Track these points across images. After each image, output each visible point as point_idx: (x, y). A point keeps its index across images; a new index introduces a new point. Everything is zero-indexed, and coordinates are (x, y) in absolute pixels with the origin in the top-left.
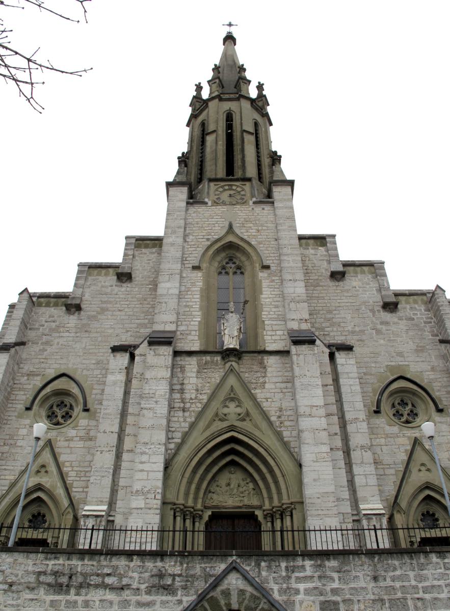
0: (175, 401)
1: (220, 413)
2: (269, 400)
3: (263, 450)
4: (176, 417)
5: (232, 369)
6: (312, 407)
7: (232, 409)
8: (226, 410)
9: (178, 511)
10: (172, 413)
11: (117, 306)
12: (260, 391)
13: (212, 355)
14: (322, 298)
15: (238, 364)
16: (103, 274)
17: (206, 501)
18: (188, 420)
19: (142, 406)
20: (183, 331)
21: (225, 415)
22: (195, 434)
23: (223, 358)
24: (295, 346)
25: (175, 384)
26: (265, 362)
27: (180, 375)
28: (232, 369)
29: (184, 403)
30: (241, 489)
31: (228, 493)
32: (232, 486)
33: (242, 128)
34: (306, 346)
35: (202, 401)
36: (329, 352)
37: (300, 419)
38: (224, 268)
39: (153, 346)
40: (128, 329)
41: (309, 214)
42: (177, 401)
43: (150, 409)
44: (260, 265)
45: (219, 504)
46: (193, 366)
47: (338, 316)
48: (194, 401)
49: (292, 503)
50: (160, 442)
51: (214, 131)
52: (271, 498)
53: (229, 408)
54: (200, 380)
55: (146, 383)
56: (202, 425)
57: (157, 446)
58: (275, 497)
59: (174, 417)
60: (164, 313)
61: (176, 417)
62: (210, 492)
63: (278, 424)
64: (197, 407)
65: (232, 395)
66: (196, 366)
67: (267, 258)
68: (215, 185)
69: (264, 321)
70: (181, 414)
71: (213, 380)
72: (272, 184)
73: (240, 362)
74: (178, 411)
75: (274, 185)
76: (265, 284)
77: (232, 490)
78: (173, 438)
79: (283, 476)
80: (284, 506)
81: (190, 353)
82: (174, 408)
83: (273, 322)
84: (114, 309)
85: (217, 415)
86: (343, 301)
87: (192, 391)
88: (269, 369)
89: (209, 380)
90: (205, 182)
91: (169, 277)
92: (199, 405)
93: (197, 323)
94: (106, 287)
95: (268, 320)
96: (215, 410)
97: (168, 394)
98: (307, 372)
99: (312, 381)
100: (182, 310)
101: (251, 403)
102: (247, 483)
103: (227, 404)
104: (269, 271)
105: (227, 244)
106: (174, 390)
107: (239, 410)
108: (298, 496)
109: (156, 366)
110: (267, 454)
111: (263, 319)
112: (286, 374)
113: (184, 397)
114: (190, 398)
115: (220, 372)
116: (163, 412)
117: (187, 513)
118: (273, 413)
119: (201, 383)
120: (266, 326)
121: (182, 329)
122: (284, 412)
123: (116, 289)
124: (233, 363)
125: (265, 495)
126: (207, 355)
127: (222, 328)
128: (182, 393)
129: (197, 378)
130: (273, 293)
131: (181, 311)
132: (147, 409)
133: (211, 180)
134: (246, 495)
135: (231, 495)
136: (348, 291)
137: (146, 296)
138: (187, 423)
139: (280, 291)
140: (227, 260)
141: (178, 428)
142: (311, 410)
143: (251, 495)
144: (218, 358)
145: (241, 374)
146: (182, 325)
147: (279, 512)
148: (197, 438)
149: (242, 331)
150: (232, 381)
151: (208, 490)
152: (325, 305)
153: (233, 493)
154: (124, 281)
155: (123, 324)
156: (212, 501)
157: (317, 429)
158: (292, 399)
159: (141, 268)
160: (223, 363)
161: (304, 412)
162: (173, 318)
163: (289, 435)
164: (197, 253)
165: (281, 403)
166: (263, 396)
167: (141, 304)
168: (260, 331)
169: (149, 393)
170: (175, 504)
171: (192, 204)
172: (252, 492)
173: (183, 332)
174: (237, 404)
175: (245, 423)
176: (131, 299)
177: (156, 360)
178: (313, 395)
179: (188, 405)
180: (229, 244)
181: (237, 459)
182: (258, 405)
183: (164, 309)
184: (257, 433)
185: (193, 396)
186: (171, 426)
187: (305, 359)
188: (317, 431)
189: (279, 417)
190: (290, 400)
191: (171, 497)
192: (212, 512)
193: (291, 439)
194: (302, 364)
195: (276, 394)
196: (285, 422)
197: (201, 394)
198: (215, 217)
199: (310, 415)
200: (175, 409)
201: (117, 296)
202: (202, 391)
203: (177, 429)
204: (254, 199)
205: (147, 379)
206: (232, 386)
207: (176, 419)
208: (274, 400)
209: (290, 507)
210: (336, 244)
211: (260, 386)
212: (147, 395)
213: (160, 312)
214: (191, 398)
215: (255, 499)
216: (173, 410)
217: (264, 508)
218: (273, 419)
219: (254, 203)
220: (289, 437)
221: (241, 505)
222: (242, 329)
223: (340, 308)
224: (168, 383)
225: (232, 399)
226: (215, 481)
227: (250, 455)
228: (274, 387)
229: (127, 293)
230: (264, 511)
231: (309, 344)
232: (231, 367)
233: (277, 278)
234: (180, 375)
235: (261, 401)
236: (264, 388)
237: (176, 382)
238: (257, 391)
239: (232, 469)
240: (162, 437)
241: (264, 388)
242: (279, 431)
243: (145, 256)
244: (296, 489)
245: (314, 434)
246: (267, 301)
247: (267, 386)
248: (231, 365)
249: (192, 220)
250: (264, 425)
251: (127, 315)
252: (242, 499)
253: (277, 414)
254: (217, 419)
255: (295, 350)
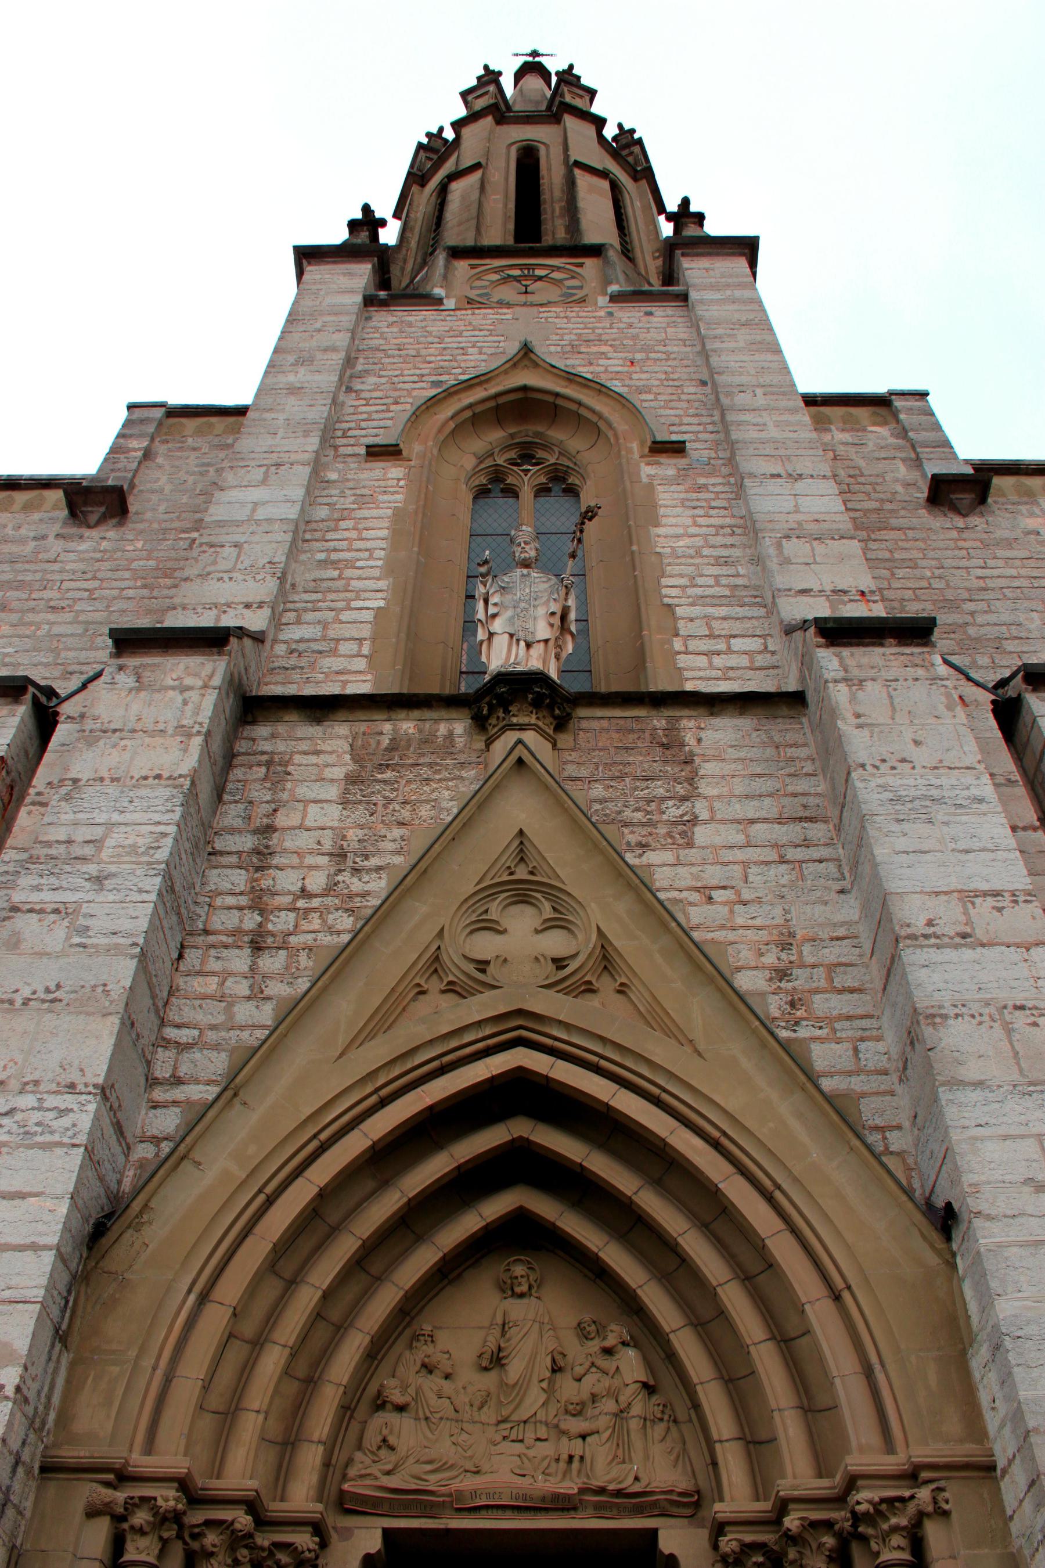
0: (219, 901)
1: (451, 955)
2: (718, 895)
3: (697, 1142)
4: (214, 974)
5: (520, 761)
6: (969, 896)
7: (522, 938)
8: (485, 946)
9: (141, 1531)
10: (192, 957)
11: (47, 594)
12: (668, 856)
13: (428, 714)
14: (911, 564)
15: (554, 746)
16: (17, 506)
17: (350, 1462)
18: (277, 989)
19: (17, 897)
20: (301, 641)
21: (482, 965)
22: (303, 1053)
23: (480, 723)
24: (832, 650)
25: (232, 831)
26: (690, 739)
27: (260, 793)
28: (520, 761)
29: (262, 912)
30: (568, 1389)
31: (489, 1415)
32: (515, 1369)
33: (567, 157)
34: (888, 651)
35: (358, 902)
36: (993, 702)
37: (912, 956)
38: (497, 476)
39: (133, 654)
40: (71, 668)
41: (823, 329)
42: (230, 901)
43: (56, 911)
44: (642, 443)
45: (433, 1482)
46: (331, 759)
47: (991, 618)
48: (316, 902)
49: (912, 1475)
50: (75, 1076)
51: (477, 166)
52: (757, 1444)
53: (504, 932)
54: (360, 814)
55: (67, 798)
56: (346, 1009)
57: (51, 1101)
58: (790, 1431)
59: (200, 973)
60: (226, 576)
61: (214, 974)
62: (380, 1404)
63: (775, 1006)
64: (331, 931)
65: (521, 873)
66: (348, 757)
67: (672, 428)
68: (473, 267)
69: (669, 605)
70: (239, 960)
71: (425, 811)
72: (678, 252)
73: (564, 739)
74: (226, 947)
75: (683, 255)
76: (667, 497)
77: (518, 1389)
78: (177, 1081)
79: (837, 1298)
80: (865, 1497)
81: (321, 708)
82: (206, 932)
83: (710, 610)
84: (32, 604)
85: (435, 964)
86: (996, 572)
87: (309, 860)
88: (708, 768)
89: (405, 814)
90: (441, 258)
91: (266, 473)
92: (346, 922)
93: (369, 616)
94: (23, 541)
95: (692, 605)
96: (427, 934)
97: (169, 842)
98: (912, 745)
99: (944, 781)
100: (308, 576)
101: (623, 906)
102: (608, 1352)
103: (495, 910)
104: (682, 462)
105: (512, 397)
106: (221, 853)
107: (556, 943)
108: (953, 1425)
109: (134, 731)
110: (728, 1168)
111: (666, 600)
112: (802, 785)
113: (265, 883)
114: (296, 888)
115: (462, 778)
116: (126, 925)
117: (211, 1539)
118: (746, 955)
119: (362, 827)
120: (681, 624)
121: (297, 637)
122: (806, 949)
123: (56, 546)
124: (530, 737)
125: (721, 1421)
126: (402, 714)
127: (481, 615)
128: (258, 869)
129: (344, 803)
130: (701, 521)
131: (302, 576)
132: (41, 911)
133: (457, 253)
134: (603, 1422)
135: (510, 1427)
136: (1009, 543)
137: (169, 565)
138: (268, 1008)
139: (734, 516)
140: (512, 454)
141: (213, 1027)
142: (966, 913)
143: (634, 1424)
144: (457, 727)
145: (568, 786)
146: (298, 622)
147: (829, 1541)
148: (313, 1079)
149: (573, 628)
150: (520, 810)
151: (372, 1389)
152: (925, 584)
153: (524, 1413)
154: (93, 518)
155: (56, 651)
156: (388, 1459)
157: (1022, 1008)
158: (842, 892)
159: (168, 488)
160: (481, 745)
161: (930, 923)
162: (266, 588)
163: (848, 1064)
164: (391, 419)
165: (787, 912)
166: (685, 876)
167: (144, 586)
168: (654, 638)
169: (69, 842)
170: (123, 1477)
171: (384, 304)
172: (637, 1409)
173: (302, 647)
174: (548, 912)
175: (593, 1002)
176: (110, 574)
177: (135, 708)
178: (962, 845)
179: (282, 922)
180: (519, 395)
181: (546, 1208)
182: (658, 914)
183: (223, 565)
184: (660, 1050)
185: (317, 882)
186: (178, 1020)
187: (891, 697)
188: (1020, 1020)
189: (782, 974)
190: (834, 896)
191: (102, 1428)
192: (388, 1534)
193: (857, 1084)
194: (879, 715)
195: (754, 870)
196: (817, 998)
197: (356, 871)
198: (465, 334)
199: (964, 936)
200: (212, 939)
201: (56, 567)
202: (367, 858)
203: (211, 1036)
204: (614, 288)
205: (75, 781)
206: (521, 832)
207: (211, 985)
208: (746, 895)
209: (902, 1500)
210: (933, 414)
211: (669, 835)
212: (60, 850)
213: (209, 574)
214: (303, 890)
215: (657, 1450)
216: (200, 940)
217: (722, 1509)
218: (746, 982)
219: (615, 298)
220: (849, 1073)
221: (569, 1486)
222: (572, 616)
223: (990, 595)
224: (179, 799)
225: (522, 893)
226: (416, 1337)
227: (622, 1179)
228: (741, 838)
229: (99, 555)
230: (719, 1528)
231: (901, 644)
232: (520, 751)
233: (720, 480)
234: (260, 793)
235: (677, 901)
236: (690, 845)
237: (238, 823)
238: (652, 857)
239: (519, 1270)
240: (91, 1048)
241: (690, 845)
242: (789, 1040)
243: (193, 455)
244: (933, 1378)
245: (1009, 1031)
246: (681, 543)
247: (702, 834)
248: (520, 742)
249: (382, 342)
250: (698, 1011)
251: (79, 623)
252: (577, 1447)
253: (770, 959)
254: (434, 985)
255: (835, 663)
